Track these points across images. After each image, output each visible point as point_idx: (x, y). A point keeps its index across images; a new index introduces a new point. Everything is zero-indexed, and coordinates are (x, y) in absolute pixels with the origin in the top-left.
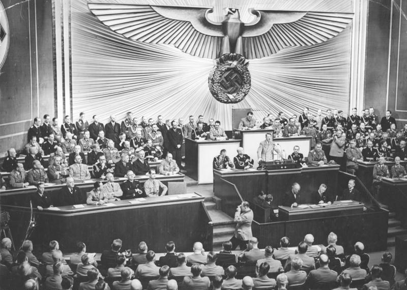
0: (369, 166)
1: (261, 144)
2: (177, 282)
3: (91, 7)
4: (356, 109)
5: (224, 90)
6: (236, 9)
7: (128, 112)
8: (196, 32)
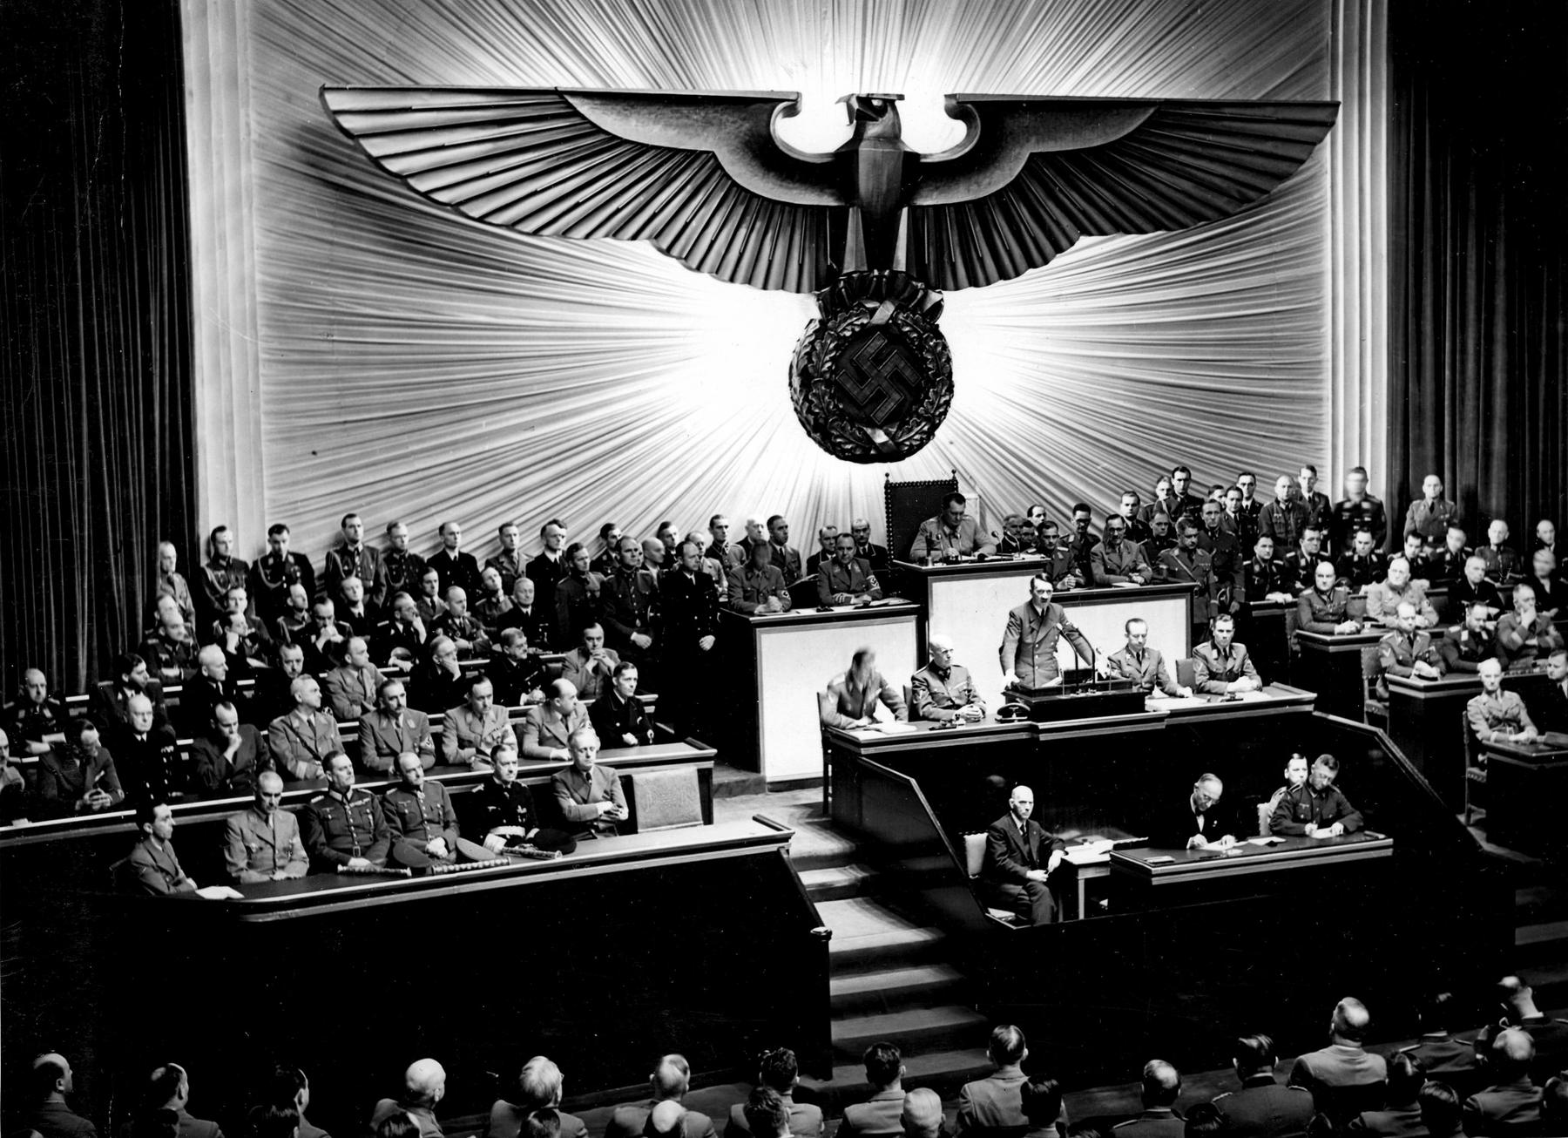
0: (1429, 695)
1: (1012, 615)
2: (942, 1100)
3: (336, 101)
4: (1361, 470)
5: (853, 410)
6: (885, 101)
8: (735, 189)
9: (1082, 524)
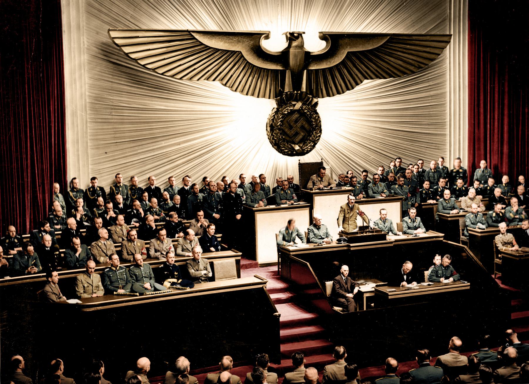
1: (341, 207)
6: (299, 34)
7: (221, 178)
9: (365, 177)
